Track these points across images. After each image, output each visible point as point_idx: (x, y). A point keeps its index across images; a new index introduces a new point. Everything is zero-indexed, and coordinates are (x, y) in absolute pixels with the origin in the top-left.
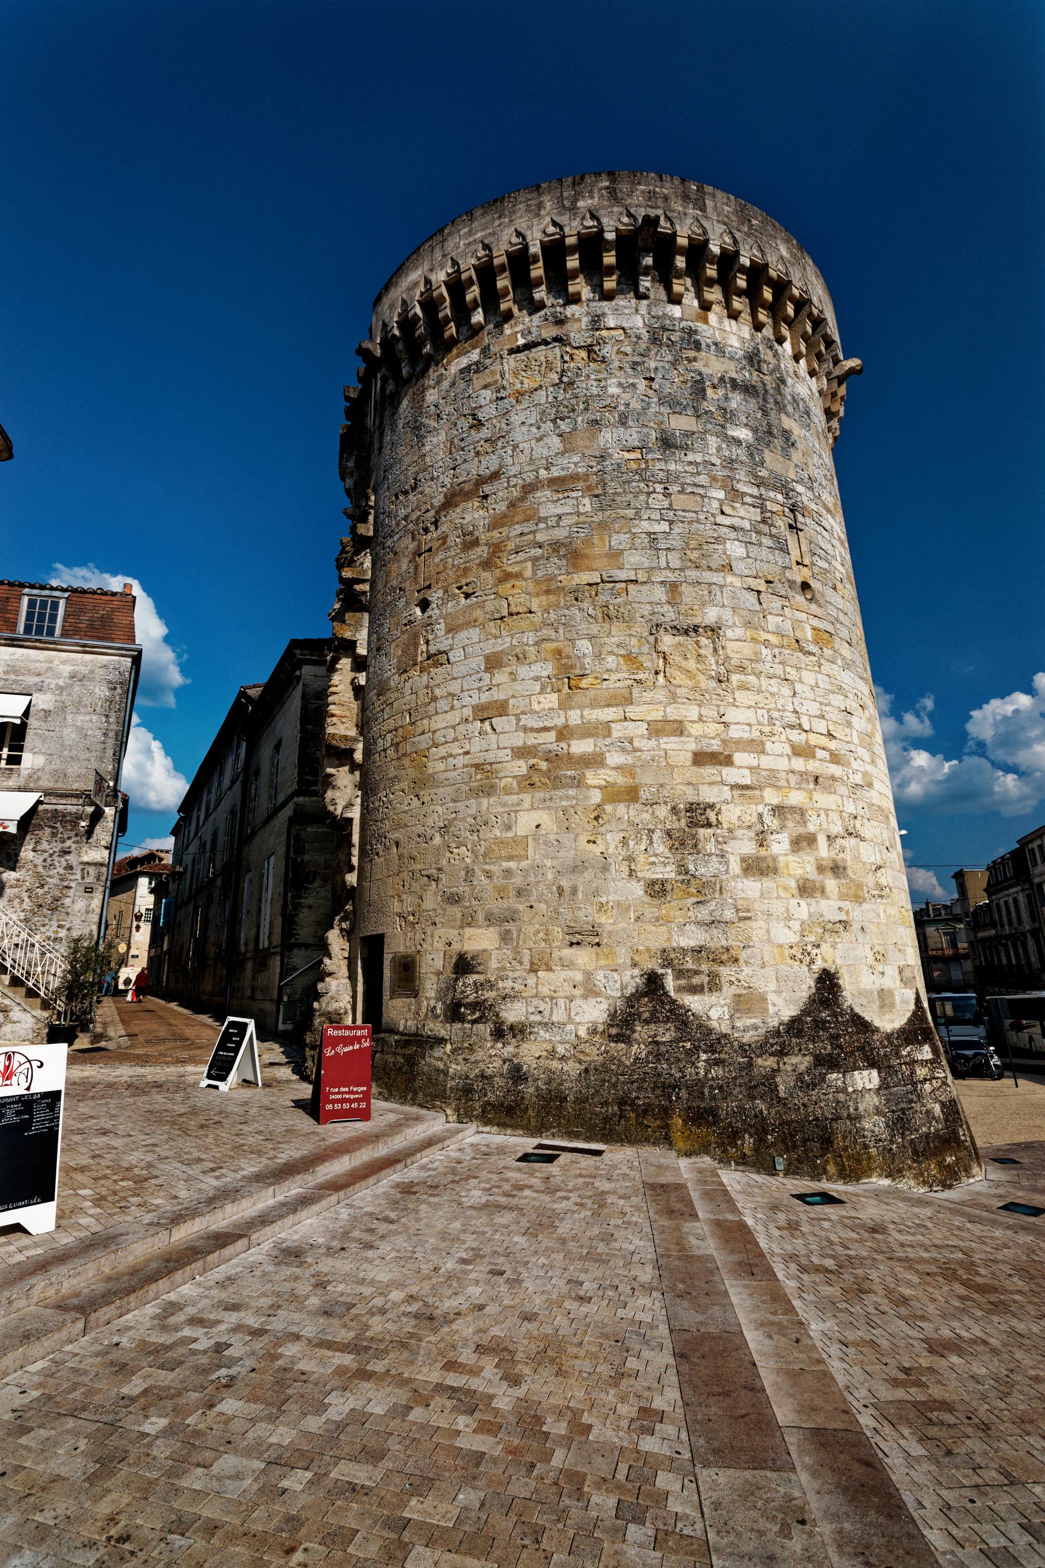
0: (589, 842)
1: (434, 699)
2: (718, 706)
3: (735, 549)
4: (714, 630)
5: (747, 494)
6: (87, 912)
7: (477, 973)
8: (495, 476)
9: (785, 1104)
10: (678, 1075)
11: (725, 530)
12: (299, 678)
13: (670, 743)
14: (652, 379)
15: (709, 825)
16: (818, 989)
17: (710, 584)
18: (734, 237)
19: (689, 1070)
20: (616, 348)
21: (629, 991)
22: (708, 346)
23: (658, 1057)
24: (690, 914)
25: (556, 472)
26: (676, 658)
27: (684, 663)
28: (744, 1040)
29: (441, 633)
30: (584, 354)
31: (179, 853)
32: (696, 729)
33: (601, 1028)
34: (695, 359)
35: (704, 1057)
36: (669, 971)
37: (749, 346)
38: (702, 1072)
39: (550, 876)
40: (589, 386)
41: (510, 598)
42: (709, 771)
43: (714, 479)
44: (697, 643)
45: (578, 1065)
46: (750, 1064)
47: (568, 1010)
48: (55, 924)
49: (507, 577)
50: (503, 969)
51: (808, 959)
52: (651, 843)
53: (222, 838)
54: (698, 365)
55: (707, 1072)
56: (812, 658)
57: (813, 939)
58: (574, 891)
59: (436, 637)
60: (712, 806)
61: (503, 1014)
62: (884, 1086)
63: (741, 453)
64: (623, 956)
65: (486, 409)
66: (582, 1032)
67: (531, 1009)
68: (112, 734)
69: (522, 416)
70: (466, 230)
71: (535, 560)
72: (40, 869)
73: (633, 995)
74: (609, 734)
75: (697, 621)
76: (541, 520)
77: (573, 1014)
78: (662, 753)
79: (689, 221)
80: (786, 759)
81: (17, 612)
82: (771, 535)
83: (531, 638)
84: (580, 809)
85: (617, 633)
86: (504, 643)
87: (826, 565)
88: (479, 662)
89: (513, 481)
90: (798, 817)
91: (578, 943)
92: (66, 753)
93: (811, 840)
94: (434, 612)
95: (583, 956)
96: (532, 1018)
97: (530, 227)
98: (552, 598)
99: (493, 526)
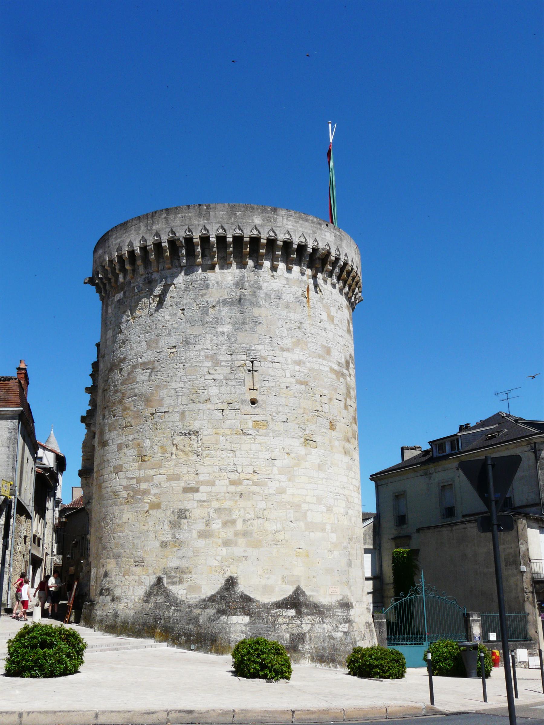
2: (195, 466)
3: (213, 391)
4: (197, 433)
11: (210, 381)
13: (174, 484)
14: (183, 310)
15: (186, 518)
17: (198, 410)
19: (167, 613)
21: (151, 584)
22: (213, 285)
25: (144, 360)
26: (180, 446)
27: (183, 448)
29: (107, 431)
32: (184, 478)
33: (142, 597)
34: (205, 294)
35: (173, 608)
38: (171, 614)
42: (189, 495)
43: (207, 357)
44: (190, 438)
46: (191, 612)
47: (133, 591)
55: (173, 614)
56: (250, 437)
58: (137, 544)
60: (188, 510)
61: (115, 593)
62: (251, 623)
63: (224, 339)
64: (151, 571)
78: (171, 488)
80: (225, 487)
87: (273, 384)
89: (130, 363)
95: (138, 570)
96: (123, 594)
97: (135, 239)
99: (123, 383)
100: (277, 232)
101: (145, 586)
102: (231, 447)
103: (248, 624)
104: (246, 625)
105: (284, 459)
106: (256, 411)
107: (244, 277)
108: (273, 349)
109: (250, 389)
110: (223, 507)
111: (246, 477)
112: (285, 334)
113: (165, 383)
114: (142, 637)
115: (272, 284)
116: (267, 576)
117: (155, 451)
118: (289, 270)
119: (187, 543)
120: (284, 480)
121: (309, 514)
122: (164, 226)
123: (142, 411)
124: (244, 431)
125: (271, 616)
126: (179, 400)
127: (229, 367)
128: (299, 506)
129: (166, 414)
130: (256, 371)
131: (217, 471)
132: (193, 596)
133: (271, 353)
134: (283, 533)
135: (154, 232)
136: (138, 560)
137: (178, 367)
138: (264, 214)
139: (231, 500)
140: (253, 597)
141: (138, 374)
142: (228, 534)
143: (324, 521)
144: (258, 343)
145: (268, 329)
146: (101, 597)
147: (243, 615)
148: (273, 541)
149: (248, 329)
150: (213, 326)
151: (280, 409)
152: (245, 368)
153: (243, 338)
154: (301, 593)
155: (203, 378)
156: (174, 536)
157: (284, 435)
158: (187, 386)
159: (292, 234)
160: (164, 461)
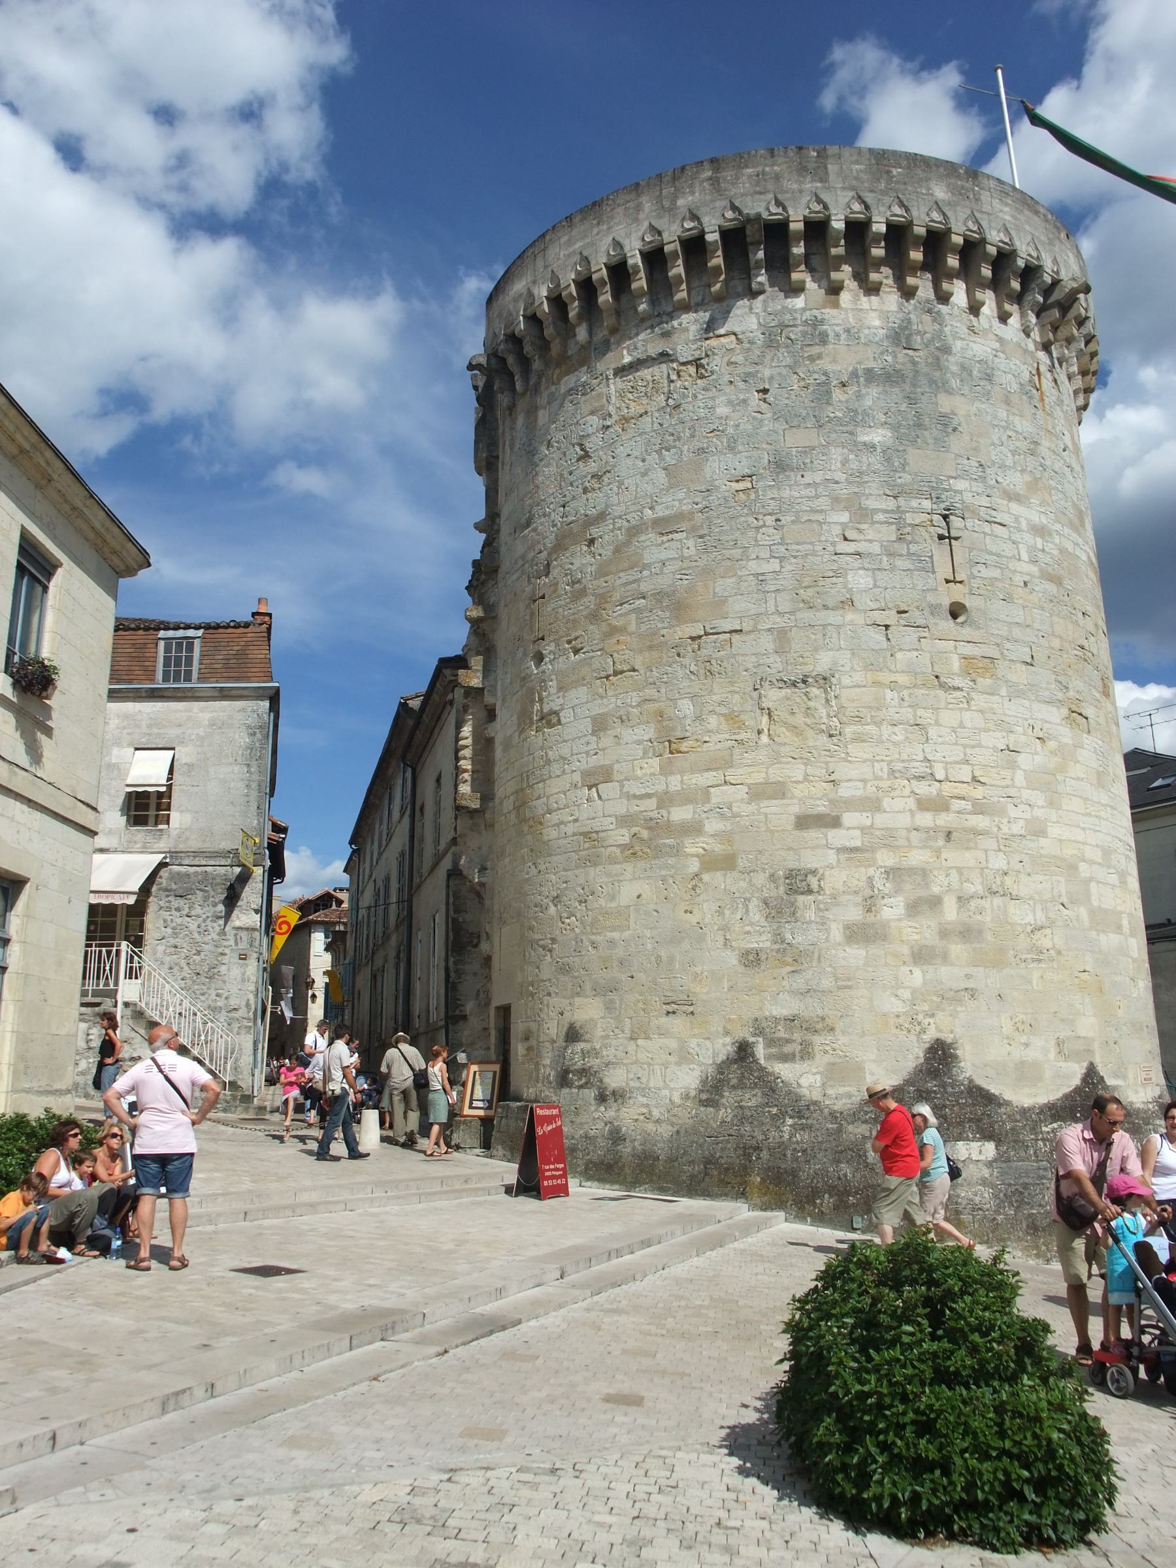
0: (686, 912)
1: (548, 762)
2: (827, 763)
3: (859, 580)
4: (825, 680)
5: (876, 511)
6: (243, 981)
7: (585, 1041)
8: (602, 517)
9: (873, 1169)
10: (761, 1137)
11: (848, 558)
12: (451, 703)
13: (771, 807)
14: (765, 391)
15: (810, 891)
16: (926, 1059)
17: (824, 626)
18: (864, 203)
20: (726, 359)
21: (719, 1060)
22: (837, 335)
23: (742, 1120)
24: (784, 983)
25: (661, 512)
26: (781, 713)
27: (791, 719)
28: (836, 1108)
29: (553, 691)
30: (692, 369)
31: (356, 893)
32: (798, 791)
33: (693, 1093)
34: (819, 356)
35: (790, 1121)
36: (761, 1040)
37: (896, 320)
38: (786, 1136)
39: (649, 946)
40: (695, 408)
41: (615, 655)
43: (836, 500)
44: (806, 694)
45: (670, 1128)
46: (840, 1131)
47: (664, 1076)
48: (213, 992)
49: (614, 631)
50: (607, 1037)
51: (918, 1028)
52: (747, 911)
53: (394, 885)
54: (825, 364)
56: (958, 694)
57: (926, 1008)
58: (671, 960)
59: (549, 695)
60: (814, 872)
61: (606, 1080)
62: (1001, 1158)
63: (875, 461)
64: (716, 1026)
65: (593, 438)
66: (677, 1099)
67: (631, 1076)
68: (254, 785)
69: (629, 446)
70: (565, 238)
71: (638, 610)
72: (196, 935)
73: (723, 1062)
74: (707, 799)
75: (807, 669)
76: (646, 567)
77: (667, 1080)
78: (762, 817)
79: (805, 199)
81: (155, 659)
82: (909, 554)
83: (634, 698)
84: (678, 877)
85: (719, 691)
86: (609, 704)
87: (996, 573)
88: (586, 726)
89: (619, 523)
90: (918, 879)
91: (674, 1013)
92: (211, 809)
93: (935, 903)
94: (547, 666)
95: (677, 1024)
96: (632, 1084)
97: (628, 235)
98: (655, 654)
99: (602, 572)
100: (984, 224)
101: (700, 1064)
102: (915, 715)
103: (995, 1160)
104: (990, 1164)
105: (1036, 753)
106: (966, 632)
107: (909, 321)
108: (988, 491)
109: (948, 581)
110: (904, 864)
111: (956, 792)
112: (1009, 462)
113: (729, 563)
114: (706, 1194)
115: (971, 344)
116: (1024, 1039)
117: (710, 727)
118: (1004, 318)
119: (816, 955)
120: (1040, 803)
121: (1094, 888)
122: (708, 198)
123: (664, 632)
124: (942, 679)
125: (1043, 1140)
126: (771, 602)
127: (894, 527)
128: (1073, 868)
129: (735, 637)
130: (956, 539)
131: (885, 776)
132: (842, 1090)
133: (985, 501)
134: (1048, 931)
135: (684, 211)
136: (674, 999)
137: (761, 523)
138: (953, 180)
139: (925, 847)
140: (997, 1093)
141: (644, 548)
142: (922, 931)
143: (1119, 908)
144: (954, 474)
145: (975, 445)
146: (566, 1091)
147: (979, 1140)
148: (1030, 951)
149: (930, 441)
150: (845, 429)
151: (1017, 632)
152: (932, 529)
153: (921, 461)
154: (1099, 1082)
155: (831, 548)
156: (778, 938)
157: (1029, 694)
158: (788, 567)
159: (1013, 233)
160: (737, 751)
